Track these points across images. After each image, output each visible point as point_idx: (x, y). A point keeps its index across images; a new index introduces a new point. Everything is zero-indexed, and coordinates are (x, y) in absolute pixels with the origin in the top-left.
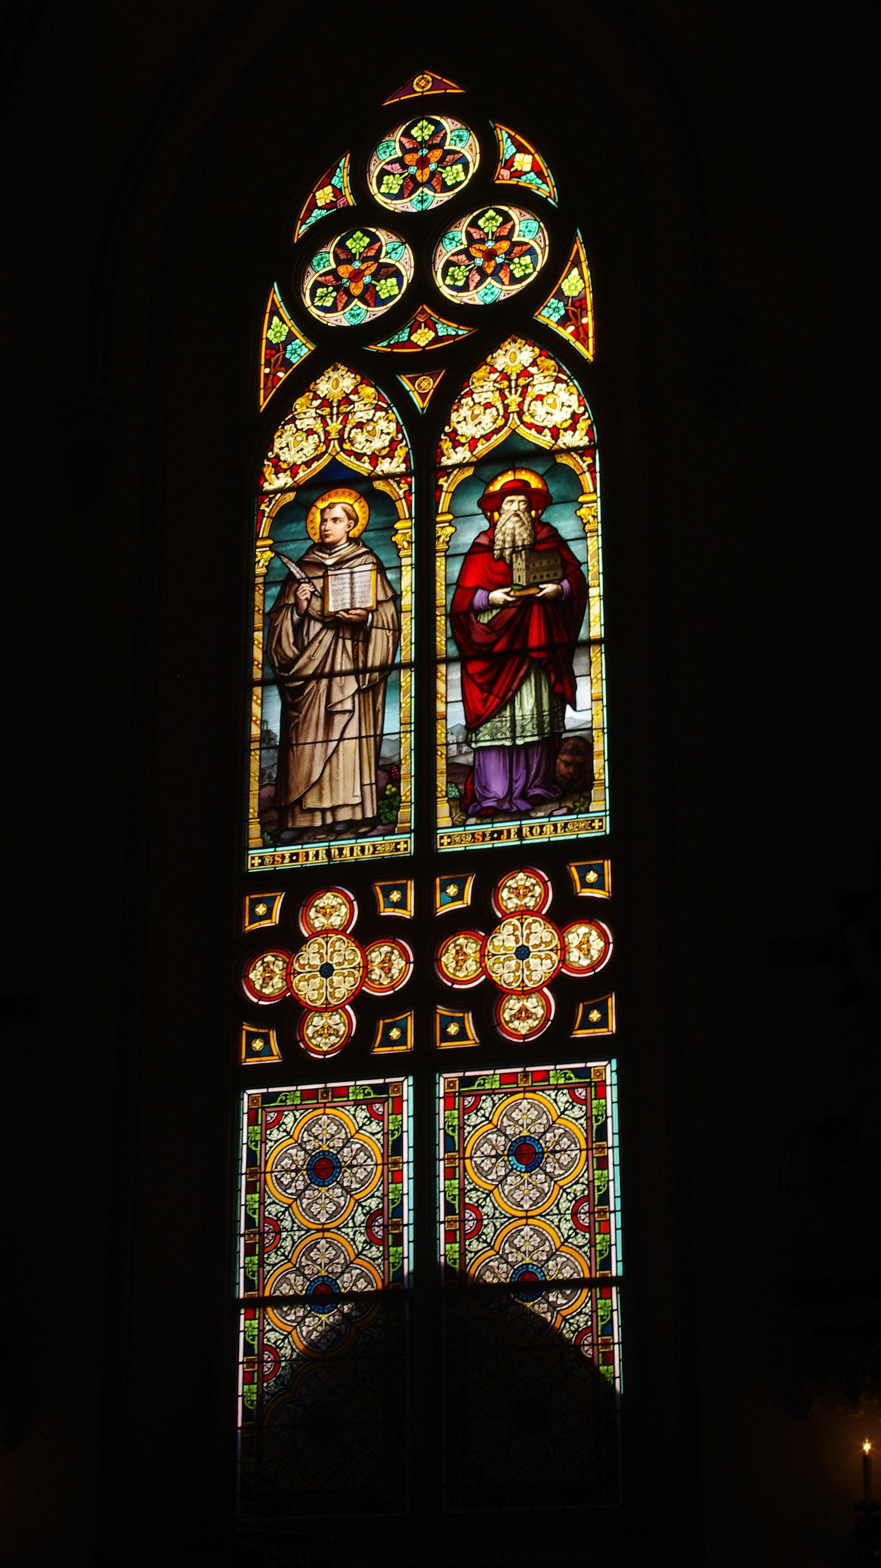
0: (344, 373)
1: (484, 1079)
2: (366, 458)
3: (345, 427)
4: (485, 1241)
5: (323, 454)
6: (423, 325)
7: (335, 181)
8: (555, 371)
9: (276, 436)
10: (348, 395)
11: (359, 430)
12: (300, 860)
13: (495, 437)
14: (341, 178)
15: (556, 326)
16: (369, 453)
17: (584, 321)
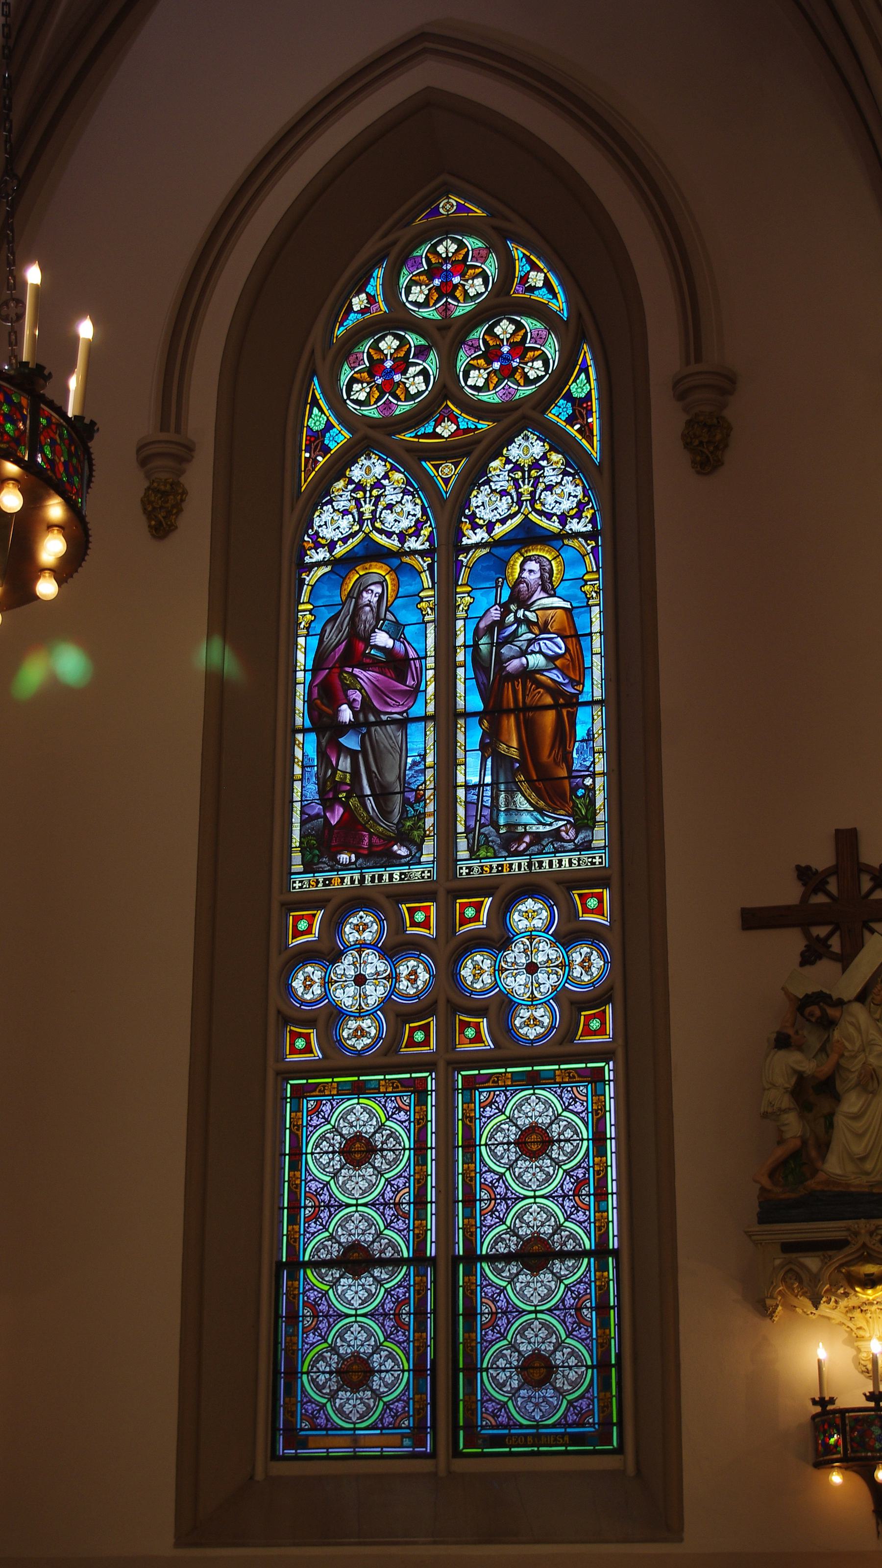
0: (375, 461)
1: (324, 1087)
2: (555, 518)
3: (377, 507)
4: (498, 1217)
5: (357, 533)
6: (446, 419)
7: (369, 289)
8: (562, 464)
9: (315, 516)
10: (537, 461)
11: (389, 511)
12: (505, 870)
13: (509, 522)
14: (375, 286)
15: (564, 424)
16: (397, 532)
17: (590, 420)
